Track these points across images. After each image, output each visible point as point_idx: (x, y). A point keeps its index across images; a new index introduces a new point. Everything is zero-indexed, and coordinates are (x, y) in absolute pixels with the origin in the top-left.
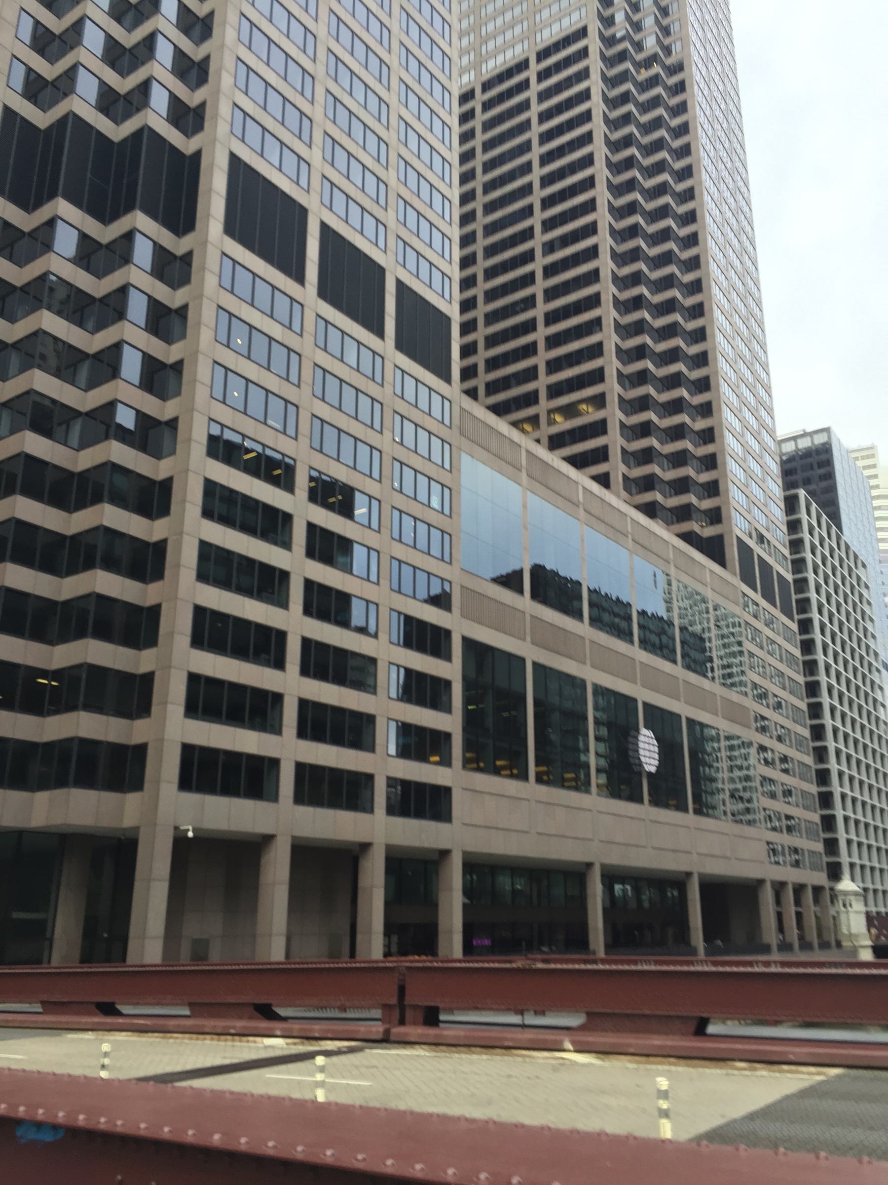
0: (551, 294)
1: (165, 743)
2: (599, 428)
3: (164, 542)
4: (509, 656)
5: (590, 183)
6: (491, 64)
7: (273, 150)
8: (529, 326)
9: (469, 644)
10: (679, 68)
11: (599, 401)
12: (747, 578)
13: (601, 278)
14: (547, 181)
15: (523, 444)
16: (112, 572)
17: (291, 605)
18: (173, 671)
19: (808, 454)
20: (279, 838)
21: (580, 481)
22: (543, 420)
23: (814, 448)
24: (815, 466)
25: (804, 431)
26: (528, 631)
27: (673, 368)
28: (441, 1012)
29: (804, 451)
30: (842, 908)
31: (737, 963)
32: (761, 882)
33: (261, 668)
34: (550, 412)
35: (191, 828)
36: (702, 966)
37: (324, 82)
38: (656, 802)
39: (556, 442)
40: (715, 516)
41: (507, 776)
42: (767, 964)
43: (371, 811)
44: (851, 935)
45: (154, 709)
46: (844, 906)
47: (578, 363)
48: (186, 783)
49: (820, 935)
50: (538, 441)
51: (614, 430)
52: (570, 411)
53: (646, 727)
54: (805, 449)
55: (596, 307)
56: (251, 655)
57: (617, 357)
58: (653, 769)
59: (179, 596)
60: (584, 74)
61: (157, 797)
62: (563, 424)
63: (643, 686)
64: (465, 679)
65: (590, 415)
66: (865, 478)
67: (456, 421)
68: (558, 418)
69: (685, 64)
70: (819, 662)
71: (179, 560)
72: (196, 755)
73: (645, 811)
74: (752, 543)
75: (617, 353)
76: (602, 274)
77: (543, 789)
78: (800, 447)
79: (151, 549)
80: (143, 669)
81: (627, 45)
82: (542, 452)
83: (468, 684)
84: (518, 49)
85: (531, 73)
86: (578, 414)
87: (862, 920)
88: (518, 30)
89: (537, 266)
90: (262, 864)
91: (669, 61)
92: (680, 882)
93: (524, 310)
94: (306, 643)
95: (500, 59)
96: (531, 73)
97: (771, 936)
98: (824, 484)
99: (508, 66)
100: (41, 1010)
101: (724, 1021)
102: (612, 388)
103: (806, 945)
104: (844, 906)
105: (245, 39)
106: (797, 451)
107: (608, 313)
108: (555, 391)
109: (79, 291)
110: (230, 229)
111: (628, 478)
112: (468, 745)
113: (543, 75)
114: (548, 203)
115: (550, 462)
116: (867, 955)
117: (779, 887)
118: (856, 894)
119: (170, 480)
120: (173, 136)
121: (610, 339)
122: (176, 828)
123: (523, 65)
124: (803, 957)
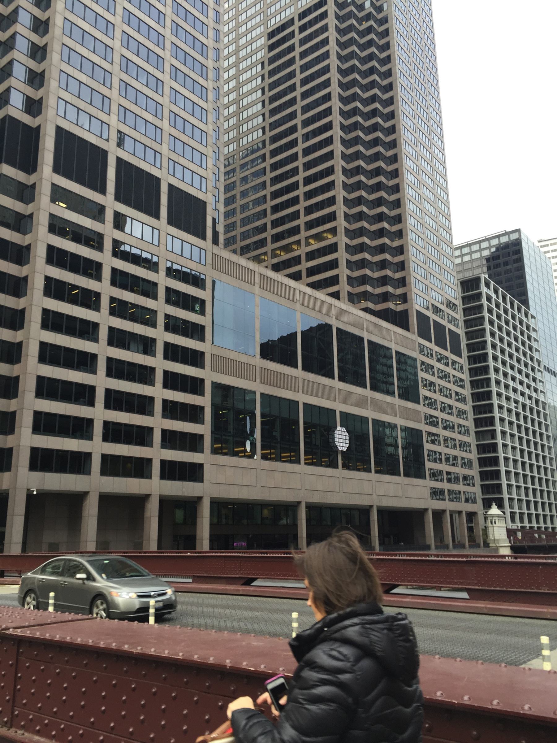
0: (308, 166)
1: (21, 448)
2: (333, 248)
3: (21, 342)
5: (328, 97)
6: (273, 21)
7: (84, 120)
9: (216, 386)
10: (385, 20)
11: (334, 231)
12: (424, 333)
13: (335, 157)
14: (305, 95)
17: (99, 372)
18: (24, 410)
19: (506, 246)
20: (91, 494)
22: (303, 242)
24: (511, 254)
27: (379, 210)
30: (490, 525)
31: (422, 555)
32: (426, 510)
34: (307, 238)
37: (118, 74)
38: (346, 466)
39: (276, 268)
40: (404, 298)
41: (242, 457)
42: (428, 555)
44: (494, 540)
45: (16, 430)
46: (492, 523)
47: (322, 208)
48: (33, 467)
49: (454, 540)
50: (267, 267)
51: (342, 248)
52: (318, 237)
53: (341, 426)
54: (505, 243)
55: (332, 174)
57: (344, 204)
58: (345, 449)
59: (27, 372)
60: (325, 28)
65: (331, 239)
66: (547, 259)
67: (209, 261)
68: (312, 241)
69: (389, 18)
73: (340, 472)
74: (428, 313)
75: (344, 202)
77: (266, 463)
78: (502, 242)
80: (12, 409)
81: (352, 8)
83: (215, 407)
84: (288, 12)
85: (295, 28)
86: (292, 250)
87: (504, 532)
88: (258, 19)
89: (299, 149)
91: (380, 16)
93: (292, 176)
95: (278, 18)
96: (295, 28)
97: (431, 539)
98: (516, 265)
99: (308, 6)
101: (78, 583)
102: (341, 223)
104: (492, 523)
106: (500, 244)
108: (310, 225)
109: (19, 182)
110: (56, 169)
112: (215, 440)
113: (303, 29)
114: (306, 109)
115: (276, 278)
116: (505, 551)
118: (499, 516)
119: (24, 309)
120: (26, 119)
121: (340, 193)
122: (28, 490)
123: (291, 22)
124: (455, 552)
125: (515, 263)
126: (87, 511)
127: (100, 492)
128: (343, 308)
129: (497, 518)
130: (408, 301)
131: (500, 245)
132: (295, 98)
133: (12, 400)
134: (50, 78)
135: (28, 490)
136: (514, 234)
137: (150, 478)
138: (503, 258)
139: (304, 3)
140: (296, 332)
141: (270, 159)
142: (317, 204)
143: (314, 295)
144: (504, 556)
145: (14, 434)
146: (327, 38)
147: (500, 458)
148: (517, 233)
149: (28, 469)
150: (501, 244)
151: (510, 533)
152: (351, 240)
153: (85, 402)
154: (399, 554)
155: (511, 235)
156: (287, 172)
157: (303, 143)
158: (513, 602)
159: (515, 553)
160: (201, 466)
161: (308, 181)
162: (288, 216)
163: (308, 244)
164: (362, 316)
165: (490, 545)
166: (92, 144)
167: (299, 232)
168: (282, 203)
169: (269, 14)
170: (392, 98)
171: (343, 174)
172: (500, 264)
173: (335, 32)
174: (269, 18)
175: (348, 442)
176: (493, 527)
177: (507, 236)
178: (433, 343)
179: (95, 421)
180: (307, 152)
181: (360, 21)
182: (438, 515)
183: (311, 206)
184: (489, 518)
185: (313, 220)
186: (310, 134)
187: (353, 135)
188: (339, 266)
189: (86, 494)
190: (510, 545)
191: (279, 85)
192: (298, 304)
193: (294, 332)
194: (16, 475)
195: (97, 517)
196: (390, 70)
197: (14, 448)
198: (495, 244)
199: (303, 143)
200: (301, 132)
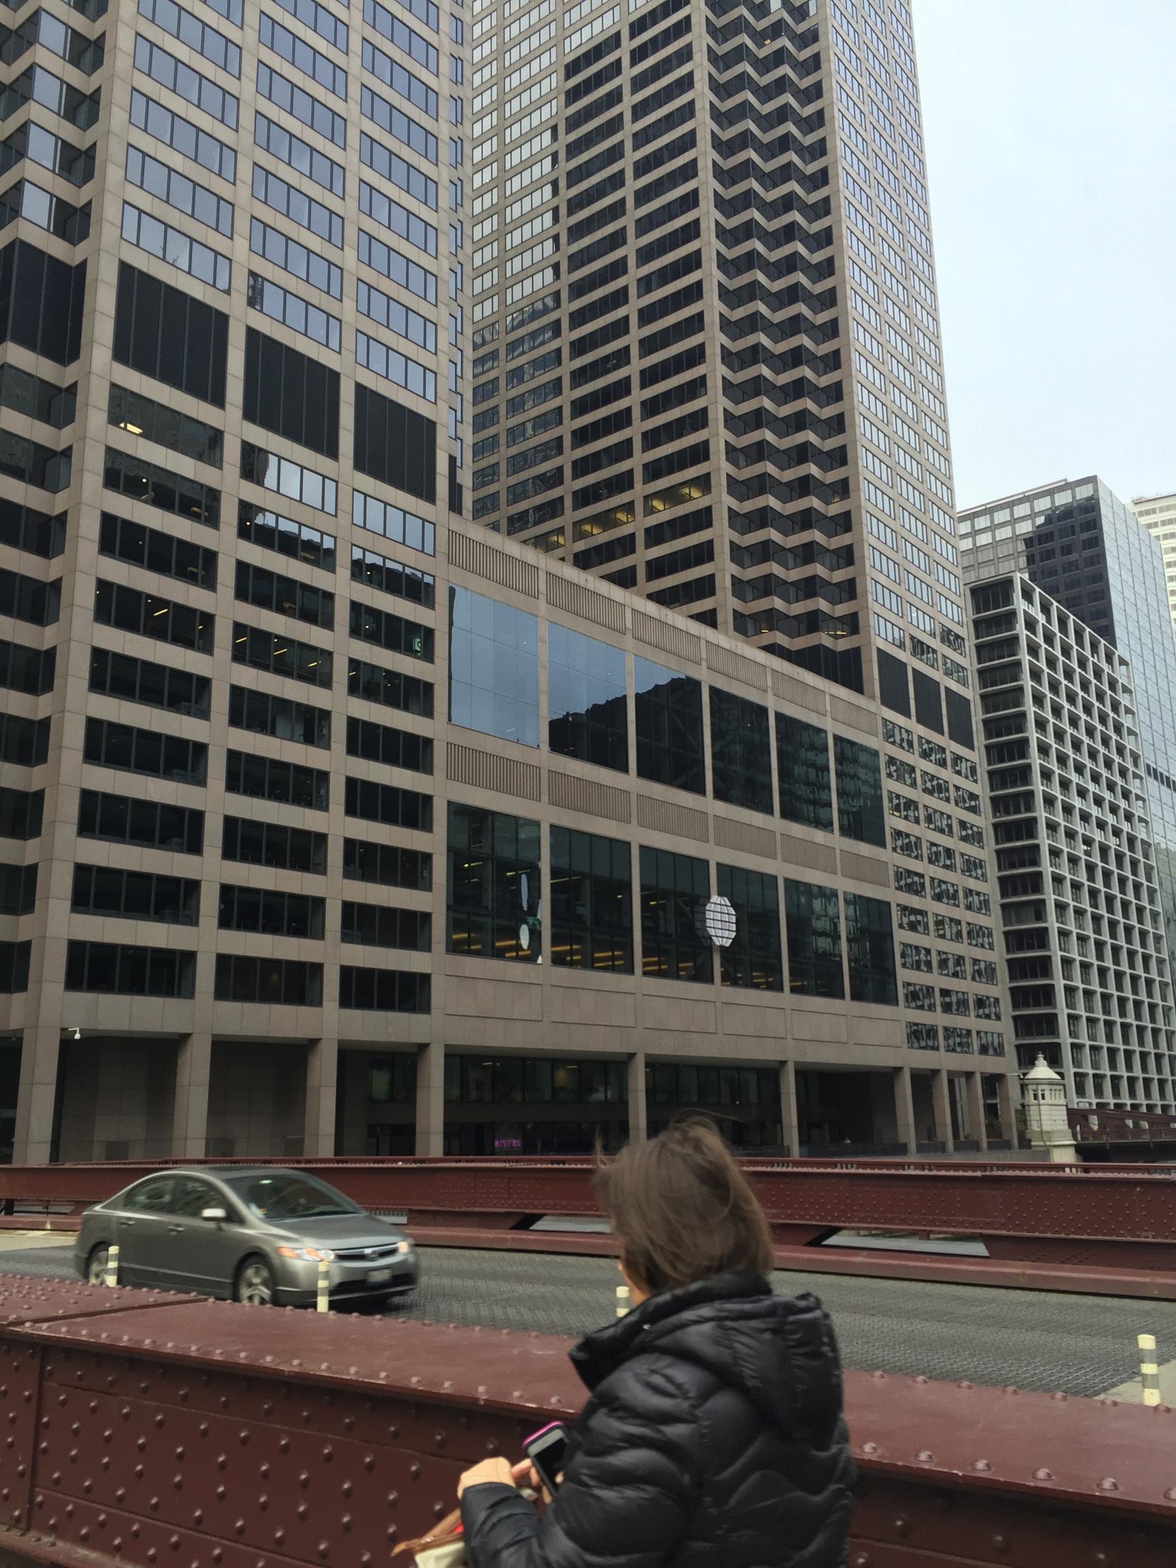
0: (649, 345)
1: (47, 941)
2: (703, 519)
3: (48, 719)
4: (515, 821)
5: (691, 200)
6: (576, 39)
7: (179, 250)
8: (622, 388)
9: (458, 811)
10: (812, 36)
11: (704, 483)
12: (894, 698)
14: (642, 196)
15: (542, 565)
16: (351, 615)
19: (1067, 513)
20: (194, 1037)
22: (639, 508)
23: (1075, 505)
24: (1077, 530)
25: (1065, 480)
26: (545, 789)
28: (71, 1254)
29: (1062, 508)
30: (1033, 1101)
32: (898, 1070)
33: (170, 854)
34: (647, 498)
35: (78, 1029)
36: (842, 1168)
37: (249, 154)
38: (730, 979)
39: (584, 561)
40: (852, 624)
42: (902, 1166)
43: (319, 1003)
44: (1042, 1132)
46: (1036, 1097)
47: (680, 435)
48: (74, 982)
50: (563, 559)
51: (721, 518)
52: (671, 496)
53: (720, 894)
56: (157, 843)
57: (726, 427)
58: (728, 943)
61: (39, 996)
63: (717, 844)
64: (451, 849)
65: (697, 501)
66: (1153, 540)
67: (442, 546)
70: (1036, 793)
71: (61, 740)
72: (87, 953)
73: (717, 991)
74: (903, 656)
76: (707, 319)
79: (36, 726)
82: (571, 573)
83: (456, 856)
85: (623, 53)
86: (618, 524)
87: (1062, 1114)
90: (179, 1063)
92: (770, 1073)
93: (616, 367)
94: (351, 783)
95: (586, 33)
96: (623, 53)
98: (1088, 553)
102: (720, 466)
104: (1036, 1097)
105: (139, 119)
106: (1054, 509)
107: (715, 370)
108: (654, 471)
111: (741, 581)
112: (454, 925)
113: (638, 55)
114: (645, 225)
115: (582, 584)
116: (1065, 1156)
117: (924, 1081)
118: (1051, 1082)
120: (57, 248)
121: (716, 403)
122: (63, 1030)
123: (614, 41)
124: (958, 1159)
125: (1084, 549)
131: (1054, 511)
135: (63, 1030)
136: (1084, 488)
140: (625, 696)
141: (571, 330)
142: (668, 425)
143: (663, 619)
148: (1091, 485)
149: (62, 985)
150: (1057, 508)
153: (182, 844)
156: (606, 359)
159: (1085, 1161)
160: (425, 978)
162: (607, 450)
163: (650, 511)
168: (595, 425)
171: (723, 362)
173: (706, 63)
174: (568, 33)
176: (1039, 1105)
178: (914, 718)
180: (647, 315)
184: (1030, 1087)
189: (184, 1038)
190: (1074, 1142)
192: (629, 638)
200: (635, 273)
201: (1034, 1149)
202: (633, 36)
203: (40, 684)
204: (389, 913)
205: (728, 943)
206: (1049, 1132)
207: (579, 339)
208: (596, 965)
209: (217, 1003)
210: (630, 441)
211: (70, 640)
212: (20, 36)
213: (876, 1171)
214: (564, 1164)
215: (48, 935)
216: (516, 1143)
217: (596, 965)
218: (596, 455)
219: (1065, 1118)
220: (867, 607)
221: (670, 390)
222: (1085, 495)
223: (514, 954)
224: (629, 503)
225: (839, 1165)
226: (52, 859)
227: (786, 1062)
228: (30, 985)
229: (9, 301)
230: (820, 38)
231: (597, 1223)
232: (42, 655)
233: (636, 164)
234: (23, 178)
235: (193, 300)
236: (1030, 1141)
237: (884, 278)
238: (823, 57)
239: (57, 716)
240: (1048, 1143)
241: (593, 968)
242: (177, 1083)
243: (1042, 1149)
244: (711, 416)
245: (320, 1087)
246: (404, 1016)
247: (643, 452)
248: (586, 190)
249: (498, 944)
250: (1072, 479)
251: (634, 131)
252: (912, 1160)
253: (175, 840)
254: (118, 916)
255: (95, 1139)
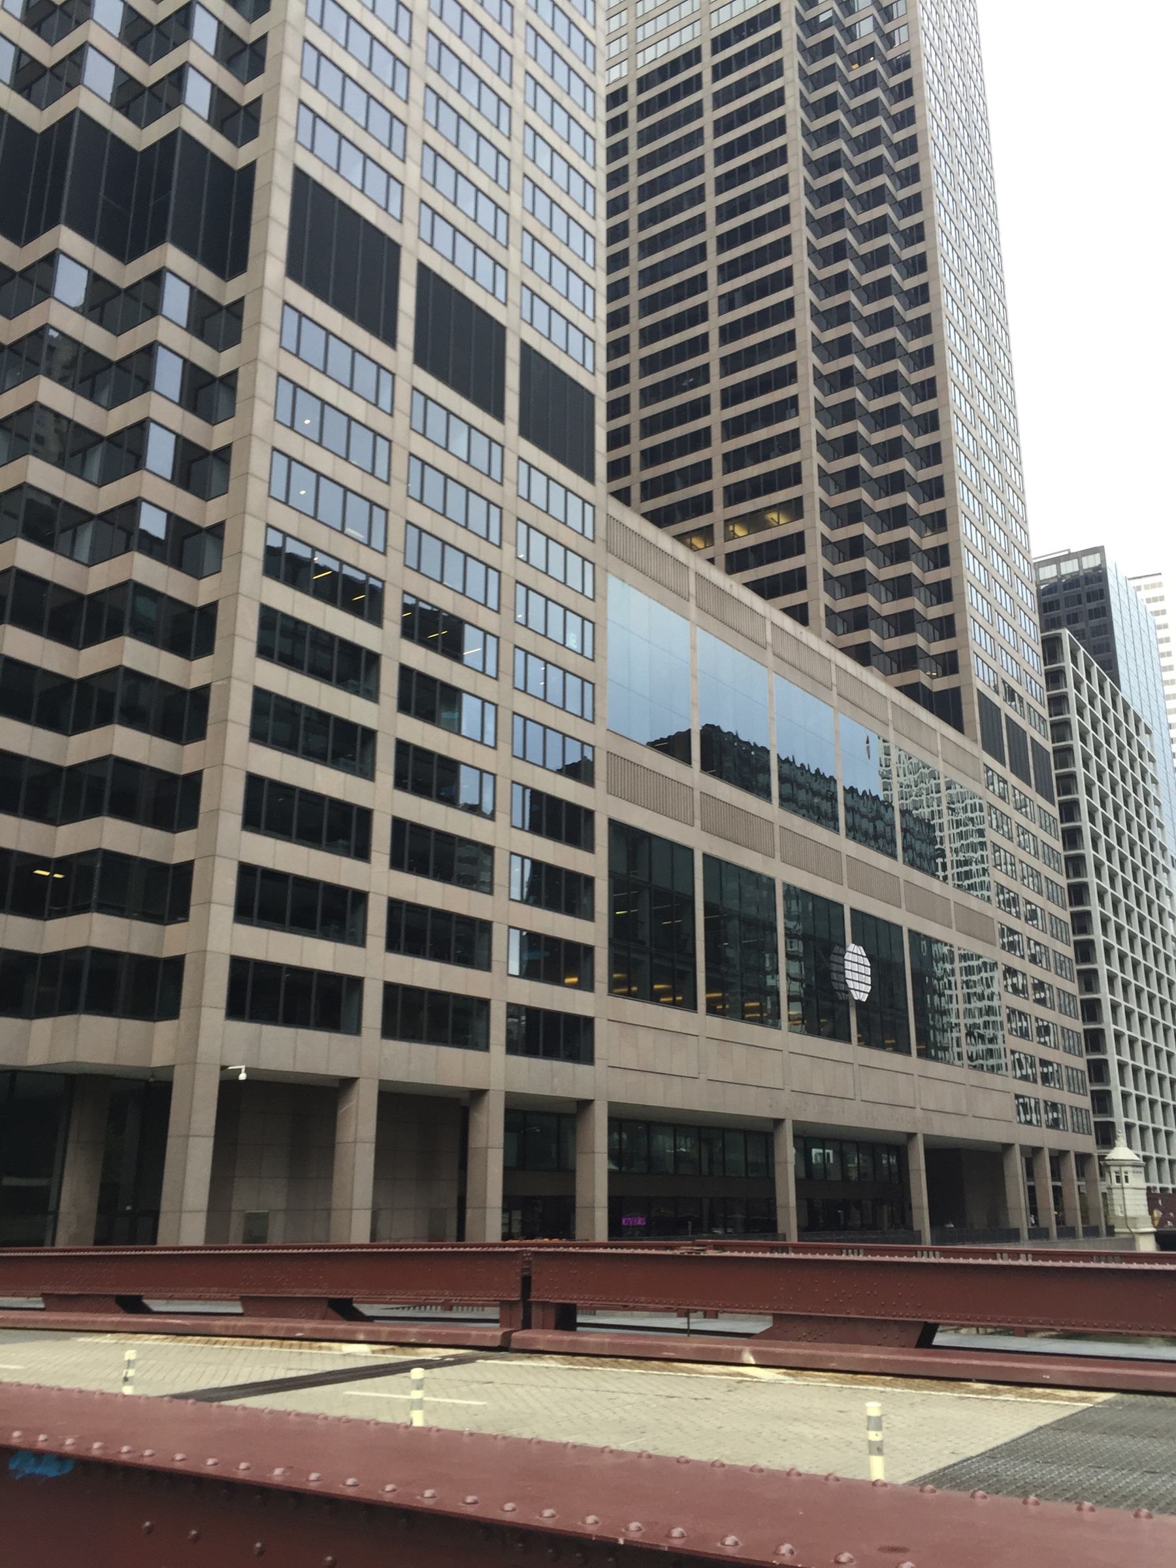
1: (209, 957)
2: (794, 544)
3: (206, 688)
5: (783, 216)
6: (650, 54)
7: (352, 165)
9: (617, 829)
10: (904, 63)
11: (795, 509)
12: (992, 745)
15: (692, 566)
19: (1074, 581)
20: (361, 1082)
21: (768, 615)
22: (719, 532)
24: (1084, 599)
27: (894, 466)
30: (1115, 1184)
32: (1008, 1147)
33: (337, 858)
34: (727, 522)
35: (243, 1067)
38: (867, 1040)
40: (950, 664)
42: (1015, 1255)
44: (1126, 1218)
46: (1118, 1180)
47: (767, 458)
48: (236, 1009)
49: (1085, 1219)
50: (711, 561)
52: (754, 521)
53: (855, 941)
55: (790, 384)
56: (324, 842)
57: (818, 450)
58: (864, 998)
59: (226, 762)
62: (745, 539)
64: (612, 875)
65: (783, 527)
68: (739, 531)
69: (913, 59)
71: (226, 712)
73: (852, 1052)
74: (998, 700)
77: (716, 1021)
78: (1063, 572)
82: (717, 576)
84: (687, 35)
86: (766, 526)
87: (1142, 1198)
89: (711, 326)
91: (890, 55)
92: (898, 1145)
93: (693, 386)
95: (662, 47)
98: (1095, 622)
99: (735, 23)
100: (239, 1310)
102: (812, 491)
103: (1066, 1232)
104: (1118, 1180)
106: (1060, 577)
108: (735, 494)
112: (615, 963)
113: (720, 71)
115: (727, 589)
116: (1147, 1245)
119: (214, 606)
120: (217, 144)
121: (808, 425)
122: (223, 1068)
123: (693, 57)
125: (1091, 618)
126: (352, 1129)
127: (381, 1081)
128: (850, 671)
129: (1129, 1169)
130: (960, 669)
131: (1060, 580)
132: (702, 217)
133: (179, 835)
134: (282, 53)
135: (223, 1068)
136: (1091, 557)
137: (486, 1048)
138: (1067, 606)
139: (737, 7)
140: (689, 731)
141: (641, 347)
142: (753, 447)
143: (798, 637)
144: (494, 1245)
145: (187, 920)
146: (781, 91)
147: (1106, 1032)
148: (1098, 555)
149: (223, 1012)
150: (1063, 577)
151: (1153, 1198)
152: (832, 529)
153: (348, 848)
154: (847, 1249)
155: (1084, 559)
156: (683, 376)
157: (720, 314)
158: (815, 1340)
159: (1162, 1249)
160: (589, 1021)
161: (731, 397)
162: (681, 472)
163: (729, 537)
164: (884, 693)
165: (1116, 1230)
166: (367, 223)
167: (710, 509)
168: (668, 445)
169: (640, 39)
170: (920, 226)
171: (816, 384)
172: (1059, 618)
173: (797, 80)
174: (641, 47)
175: (869, 980)
176: (1123, 1188)
177: (1076, 561)
178: (1008, 766)
179: (371, 896)
180: (729, 333)
181: (850, 59)
182: (1032, 1154)
183: (738, 452)
184: (1113, 1169)
185: (743, 482)
186: (737, 295)
187: (838, 300)
188: (809, 585)
189: (348, 1083)
190: (1154, 1230)
191: (663, 190)
192: (769, 654)
193: (684, 730)
194: (196, 1027)
195: (373, 1146)
196: (916, 167)
197: (187, 960)
198: (1048, 576)
199: (720, 314)
200: (715, 290)
201: (1117, 1237)
202: (715, 51)
203: (193, 645)
204: (301, 976)
205: (864, 998)
206: (1134, 1218)
207: (650, 356)
208: (747, 1016)
209: (384, 1041)
210: (708, 462)
211: (238, 593)
212: (66, 13)
213: (961, 1261)
214: (995, 1258)
215: (209, 948)
216: (640, 1221)
217: (747, 1016)
218: (669, 476)
219: (1146, 1202)
220: (968, 646)
221: (672, 441)
222: (1070, 571)
223: (670, 999)
224: (707, 527)
225: (919, 1253)
226: (214, 856)
227: (914, 1135)
228: (182, 1011)
229: (169, 198)
230: (912, 64)
231: (742, 1320)
232: (196, 613)
233: (718, 180)
234: (187, 62)
235: (367, 222)
236: (1113, 1227)
237: (969, 310)
238: (915, 85)
239: (220, 683)
240: (1133, 1230)
241: (743, 1019)
242: (337, 1140)
243: (1125, 1236)
244: (803, 439)
245: (487, 1148)
246: (569, 1066)
247: (724, 474)
248: (661, 205)
249: (656, 987)
250: (1074, 549)
251: (716, 146)
252: (1026, 1248)
253: (341, 841)
254: (283, 930)
255: (234, 1208)
